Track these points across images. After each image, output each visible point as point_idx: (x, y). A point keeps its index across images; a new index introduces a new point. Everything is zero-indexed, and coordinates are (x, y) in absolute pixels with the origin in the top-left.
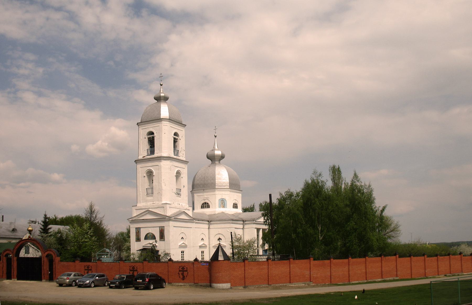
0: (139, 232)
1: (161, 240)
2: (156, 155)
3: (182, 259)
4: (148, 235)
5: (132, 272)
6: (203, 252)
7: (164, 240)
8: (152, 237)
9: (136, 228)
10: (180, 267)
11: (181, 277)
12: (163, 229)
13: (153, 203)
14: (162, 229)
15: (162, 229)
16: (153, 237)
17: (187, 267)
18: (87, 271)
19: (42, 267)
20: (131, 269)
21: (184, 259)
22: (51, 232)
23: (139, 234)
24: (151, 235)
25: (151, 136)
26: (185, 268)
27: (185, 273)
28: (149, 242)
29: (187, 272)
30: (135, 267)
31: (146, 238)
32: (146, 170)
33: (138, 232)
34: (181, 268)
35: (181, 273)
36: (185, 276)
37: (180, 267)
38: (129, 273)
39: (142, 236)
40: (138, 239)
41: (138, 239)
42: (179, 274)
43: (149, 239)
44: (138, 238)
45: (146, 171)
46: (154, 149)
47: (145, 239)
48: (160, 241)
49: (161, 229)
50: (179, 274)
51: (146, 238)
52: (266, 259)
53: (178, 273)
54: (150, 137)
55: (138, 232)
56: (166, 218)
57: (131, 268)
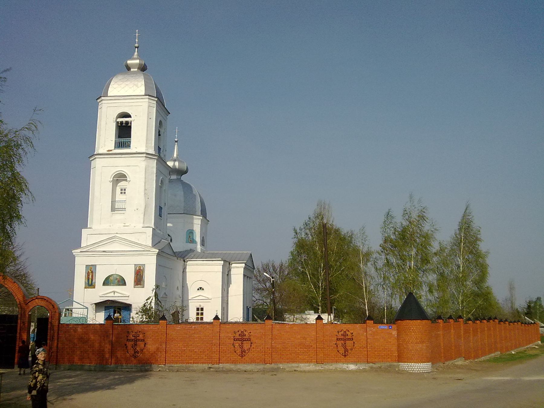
0: (92, 272)
1: (137, 286)
2: (132, 149)
3: (197, 319)
4: (111, 278)
5: (240, 342)
6: (202, 309)
7: (144, 287)
8: (119, 281)
9: (86, 265)
10: (338, 332)
11: (342, 351)
12: (142, 268)
13: (124, 225)
14: (140, 269)
15: (140, 269)
16: (122, 282)
17: (352, 332)
18: (133, 343)
19: (18, 335)
20: (237, 336)
21: (202, 319)
22: (187, 167)
23: (92, 276)
24: (117, 279)
25: (124, 120)
26: (349, 333)
27: (349, 343)
28: (112, 291)
29: (352, 342)
30: (347, 333)
31: (106, 282)
32: (115, 171)
33: (90, 272)
34: (340, 333)
35: (340, 343)
36: (349, 348)
37: (338, 332)
38: (126, 345)
39: (99, 279)
40: (90, 284)
41: (90, 284)
42: (337, 346)
43: (112, 284)
44: (90, 283)
45: (115, 173)
46: (131, 140)
47: (104, 284)
48: (134, 287)
49: (138, 269)
50: (337, 346)
51: (106, 282)
52: (213, 320)
53: (336, 344)
54: (122, 123)
55: (90, 272)
56: (151, 251)
57: (238, 334)
